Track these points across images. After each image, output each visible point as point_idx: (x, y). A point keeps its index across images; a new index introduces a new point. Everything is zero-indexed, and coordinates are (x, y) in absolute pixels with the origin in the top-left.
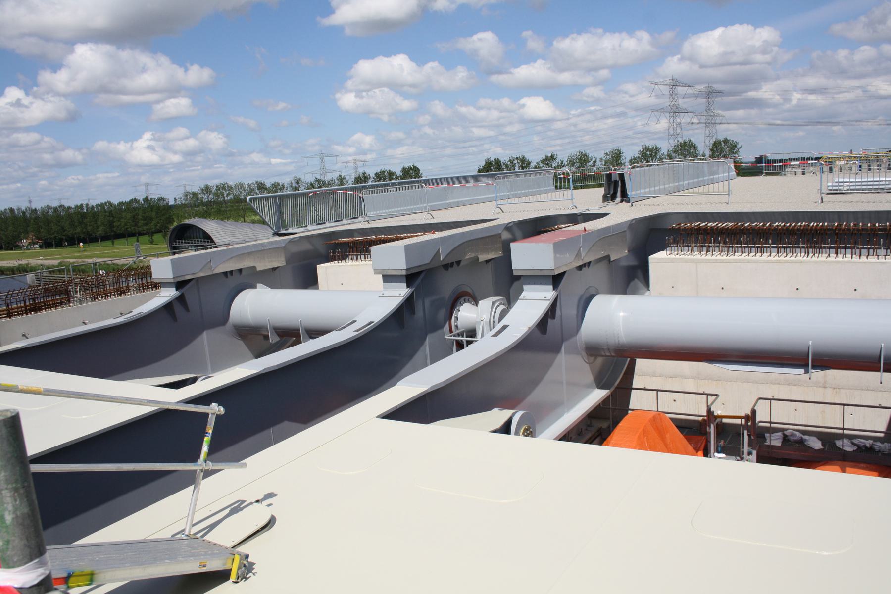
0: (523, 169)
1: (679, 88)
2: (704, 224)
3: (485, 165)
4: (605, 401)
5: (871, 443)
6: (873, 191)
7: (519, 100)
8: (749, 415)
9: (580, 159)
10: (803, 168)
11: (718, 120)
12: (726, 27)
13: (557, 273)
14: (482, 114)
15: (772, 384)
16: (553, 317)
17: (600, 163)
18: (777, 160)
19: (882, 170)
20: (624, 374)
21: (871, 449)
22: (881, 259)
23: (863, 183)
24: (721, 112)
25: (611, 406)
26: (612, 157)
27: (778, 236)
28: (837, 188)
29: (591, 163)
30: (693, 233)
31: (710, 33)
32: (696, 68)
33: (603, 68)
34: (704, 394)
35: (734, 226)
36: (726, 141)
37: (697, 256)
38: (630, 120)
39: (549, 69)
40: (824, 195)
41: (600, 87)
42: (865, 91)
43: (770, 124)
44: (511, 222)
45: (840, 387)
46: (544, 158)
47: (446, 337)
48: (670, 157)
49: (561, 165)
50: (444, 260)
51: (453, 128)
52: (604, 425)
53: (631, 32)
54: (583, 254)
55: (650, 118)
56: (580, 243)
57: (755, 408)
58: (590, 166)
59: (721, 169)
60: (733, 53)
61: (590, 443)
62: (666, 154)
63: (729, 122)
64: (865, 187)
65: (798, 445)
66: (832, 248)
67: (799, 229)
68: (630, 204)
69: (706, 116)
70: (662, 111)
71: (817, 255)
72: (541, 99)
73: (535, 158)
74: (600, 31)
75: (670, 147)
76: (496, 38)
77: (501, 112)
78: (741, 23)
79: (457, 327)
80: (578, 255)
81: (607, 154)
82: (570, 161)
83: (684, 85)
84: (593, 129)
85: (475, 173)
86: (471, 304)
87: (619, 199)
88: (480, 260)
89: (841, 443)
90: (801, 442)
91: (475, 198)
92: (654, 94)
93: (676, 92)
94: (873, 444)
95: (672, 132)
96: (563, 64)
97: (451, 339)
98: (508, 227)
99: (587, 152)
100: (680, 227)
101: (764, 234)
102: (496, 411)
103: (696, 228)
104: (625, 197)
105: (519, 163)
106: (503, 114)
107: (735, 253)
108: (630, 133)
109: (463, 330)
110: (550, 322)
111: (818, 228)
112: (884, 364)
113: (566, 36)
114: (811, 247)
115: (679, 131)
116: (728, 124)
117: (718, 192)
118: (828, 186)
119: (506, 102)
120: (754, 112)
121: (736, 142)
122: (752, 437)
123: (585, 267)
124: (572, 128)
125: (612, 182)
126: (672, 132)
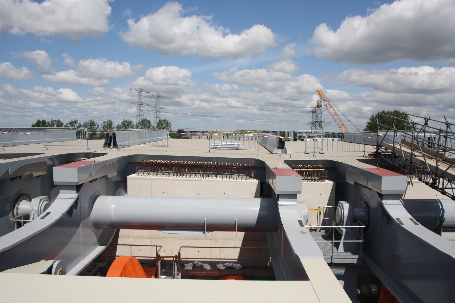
0: (58, 126)
1: (143, 93)
2: (155, 161)
3: (36, 123)
4: (103, 253)
7: (58, 89)
8: (177, 255)
9: (90, 124)
10: (199, 136)
11: (161, 110)
12: (166, 66)
13: (79, 184)
14: (36, 94)
15: (187, 239)
16: (76, 208)
18: (188, 131)
19: (233, 139)
20: (114, 237)
21: (232, 268)
23: (227, 145)
24: (162, 107)
25: (106, 255)
26: (107, 124)
27: (190, 168)
28: (216, 146)
29: (96, 126)
30: (150, 165)
31: (159, 68)
32: (151, 84)
33: (106, 78)
34: (154, 246)
35: (170, 162)
36: (165, 120)
37: (151, 176)
38: (118, 106)
39: (76, 75)
40: (210, 149)
41: (103, 88)
42: (226, 103)
43: (185, 114)
44: (53, 156)
46: (71, 121)
47: (11, 220)
48: (137, 126)
49: (80, 126)
50: (11, 175)
51: (18, 100)
52: (103, 265)
53: (121, 63)
54: (93, 174)
55: (128, 106)
56: (92, 169)
57: (180, 252)
58: (96, 128)
59: (164, 134)
60: (169, 79)
61: (95, 276)
62: (135, 124)
63: (166, 111)
64: (228, 147)
65: (200, 268)
67: (199, 165)
68: (118, 149)
69: (155, 108)
70: (134, 103)
71: (207, 177)
72: (70, 90)
73: (65, 121)
74: (105, 59)
75: (137, 121)
76: (47, 55)
77: (48, 95)
78: (174, 66)
79: (17, 214)
80: (91, 174)
81: (105, 122)
82: (85, 125)
83: (145, 92)
84: (98, 109)
85: (30, 127)
86: (27, 200)
87: (112, 146)
88: (34, 176)
89: (219, 266)
90: (201, 266)
91: (31, 141)
92: (130, 94)
93: (141, 94)
94: (232, 265)
95: (138, 114)
96: (85, 73)
97: (14, 221)
98: (51, 158)
99: (94, 120)
100: (143, 162)
101: (184, 167)
102: (43, 261)
103: (151, 162)
104: (115, 145)
105: (56, 123)
106: (49, 96)
107: (170, 175)
108: (117, 113)
109: (22, 215)
110: (74, 210)
111: (208, 165)
112: (237, 228)
113: (86, 59)
114: (205, 174)
115: (142, 114)
116: (166, 112)
117: (162, 145)
118: (212, 145)
119: (50, 90)
120: (178, 108)
122: (179, 266)
123: (94, 181)
124: (87, 107)
125: (109, 137)
126: (138, 114)
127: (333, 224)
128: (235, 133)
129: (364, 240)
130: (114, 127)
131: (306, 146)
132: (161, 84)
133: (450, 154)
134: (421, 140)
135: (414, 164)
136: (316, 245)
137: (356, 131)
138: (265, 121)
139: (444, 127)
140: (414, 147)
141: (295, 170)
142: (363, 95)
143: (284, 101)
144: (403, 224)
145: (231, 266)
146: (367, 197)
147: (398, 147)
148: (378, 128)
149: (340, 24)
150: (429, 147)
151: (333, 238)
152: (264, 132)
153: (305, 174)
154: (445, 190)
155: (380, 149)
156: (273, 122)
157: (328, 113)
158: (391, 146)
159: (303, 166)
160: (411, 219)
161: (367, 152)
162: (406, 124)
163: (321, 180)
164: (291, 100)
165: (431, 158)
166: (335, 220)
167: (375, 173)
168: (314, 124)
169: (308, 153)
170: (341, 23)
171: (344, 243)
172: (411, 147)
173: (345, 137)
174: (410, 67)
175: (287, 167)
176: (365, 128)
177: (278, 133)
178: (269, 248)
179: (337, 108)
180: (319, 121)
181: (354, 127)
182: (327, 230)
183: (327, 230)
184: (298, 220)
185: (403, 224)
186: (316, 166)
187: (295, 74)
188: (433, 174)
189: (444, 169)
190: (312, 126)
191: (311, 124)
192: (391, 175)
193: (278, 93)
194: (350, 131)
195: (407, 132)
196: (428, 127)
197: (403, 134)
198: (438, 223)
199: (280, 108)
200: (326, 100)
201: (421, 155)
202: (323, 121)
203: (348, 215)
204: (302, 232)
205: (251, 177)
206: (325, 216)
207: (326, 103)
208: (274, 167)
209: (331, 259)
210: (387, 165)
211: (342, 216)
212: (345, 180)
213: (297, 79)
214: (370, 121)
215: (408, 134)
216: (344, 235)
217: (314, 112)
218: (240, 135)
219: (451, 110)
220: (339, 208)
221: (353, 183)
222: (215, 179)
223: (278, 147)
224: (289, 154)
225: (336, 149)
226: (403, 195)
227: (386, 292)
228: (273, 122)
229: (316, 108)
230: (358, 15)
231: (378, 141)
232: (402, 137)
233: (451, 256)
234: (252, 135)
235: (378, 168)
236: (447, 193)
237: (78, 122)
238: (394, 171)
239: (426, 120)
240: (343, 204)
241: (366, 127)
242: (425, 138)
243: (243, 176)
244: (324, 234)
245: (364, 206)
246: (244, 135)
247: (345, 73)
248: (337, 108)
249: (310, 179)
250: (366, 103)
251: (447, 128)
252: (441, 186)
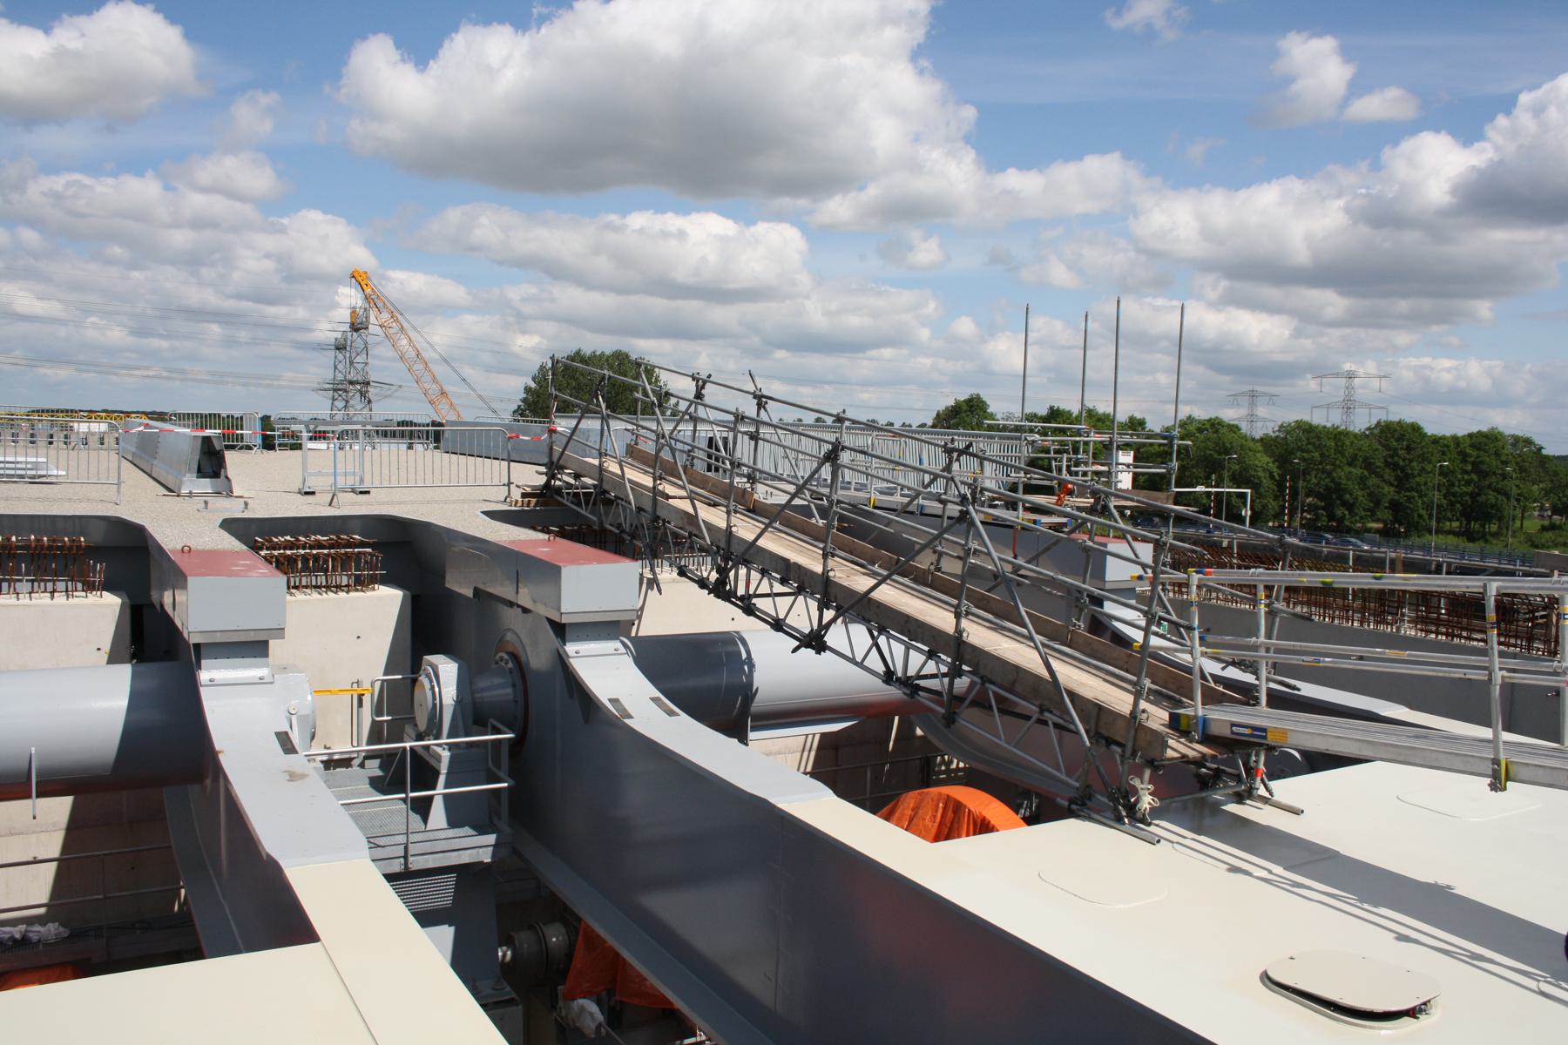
5: (23, 930)
6: (16, 479)
19: (21, 443)
21: (24, 941)
22: (24, 599)
94: (26, 931)
127: (405, 735)
128: (29, 420)
129: (512, 782)
131: (304, 469)
133: (770, 490)
134: (687, 448)
135: (664, 524)
136: (344, 815)
137: (486, 416)
139: (750, 409)
140: (664, 470)
141: (263, 553)
142: (515, 293)
143: (231, 304)
144: (630, 717)
145: (18, 936)
146: (518, 637)
147: (613, 467)
148: (551, 406)
149: (440, 46)
150: (709, 470)
152: (150, 418)
153: (300, 565)
154: (754, 601)
155: (559, 476)
157: (392, 353)
158: (594, 465)
159: (293, 539)
160: (654, 700)
161: (517, 486)
162: (639, 395)
163: (359, 588)
165: (715, 505)
166: (412, 721)
167: (540, 557)
168: (340, 390)
169: (313, 493)
170: (443, 41)
171: (445, 796)
172: (654, 467)
173: (446, 435)
174: (663, 212)
175: (230, 543)
176: (519, 407)
177: (204, 420)
178: (174, 847)
179: (422, 336)
180: (360, 379)
181: (481, 403)
182: (386, 759)
183: (386, 759)
184: (277, 734)
185: (630, 717)
186: (340, 538)
187: (274, 208)
188: (718, 551)
189: (750, 537)
190: (336, 397)
191: (329, 390)
192: (589, 561)
193: (206, 273)
194: (468, 416)
195: (641, 419)
196: (705, 406)
197: (630, 427)
198: (738, 706)
199: (215, 328)
201: (683, 493)
202: (372, 379)
204: (291, 776)
205: (90, 587)
206: (378, 711)
207: (385, 316)
208: (179, 547)
209: (406, 857)
210: (580, 527)
211: (435, 705)
212: (444, 583)
213: (282, 224)
214: (533, 385)
215: (644, 428)
216: (444, 770)
217: (340, 347)
218: (52, 426)
219: (781, 354)
220: (423, 679)
221: (469, 593)
223: (199, 471)
224: (241, 497)
225: (412, 477)
226: (634, 624)
227: (592, 939)
229: (350, 334)
230: (504, 24)
231: (551, 449)
232: (629, 438)
233: (772, 800)
234: (103, 427)
235: (552, 538)
236: (758, 610)
238: (605, 549)
239: (701, 383)
240: (437, 666)
242: (697, 440)
243: (57, 583)
244: (379, 773)
245: (510, 668)
246: (69, 429)
247: (454, 215)
248: (422, 336)
249: (319, 584)
250: (522, 322)
251: (759, 409)
252: (741, 591)
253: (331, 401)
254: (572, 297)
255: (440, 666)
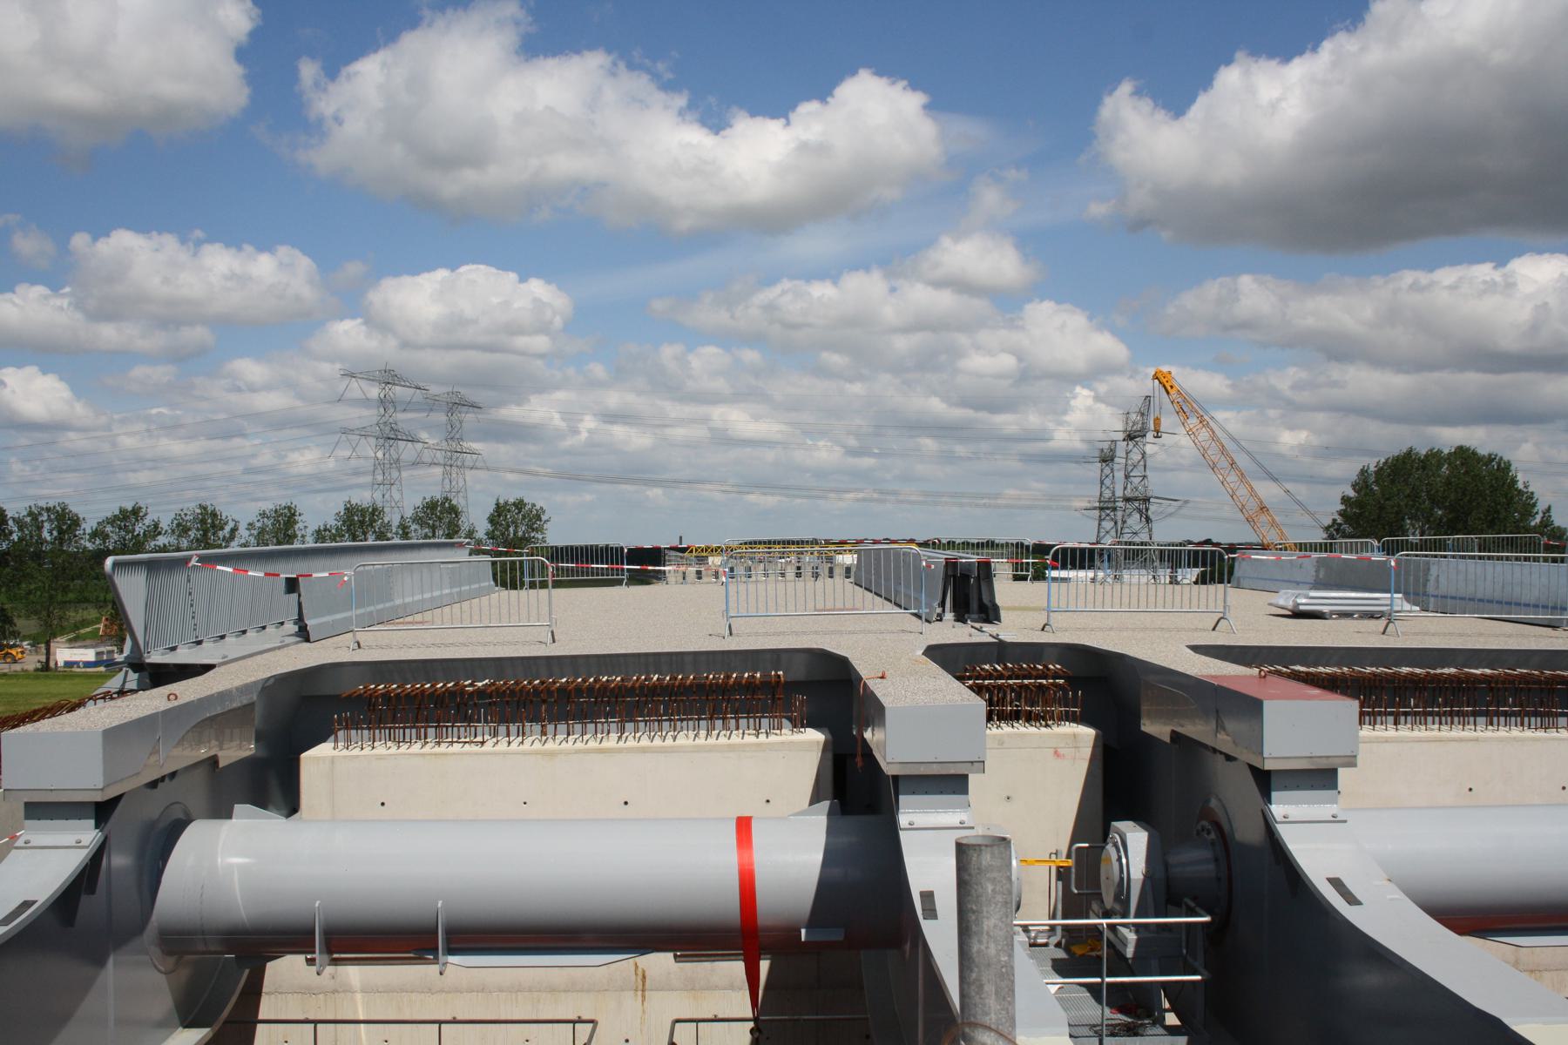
17: (247, 533)
24: (475, 446)
45: (315, 992)
62: (396, 522)
66: (1560, 716)
71: (715, 733)
82: (179, 525)
121: (542, 508)
130: (303, 532)
132: (435, 347)
138: (864, 500)
143: (959, 413)
151: (1101, 969)
156: (902, 502)
164: (977, 406)
166: (1099, 897)
168: (1108, 508)
176: (1334, 520)
199: (929, 444)
200: (1193, 411)
203: (1145, 876)
211: (1122, 879)
214: (1351, 493)
217: (1107, 459)
222: (690, 741)
228: (902, 502)
233: (1506, 1021)
237: (146, 514)
241: (1337, 517)
245: (1213, 840)
253: (1097, 523)
254: (1364, 382)
255: (1128, 835)
